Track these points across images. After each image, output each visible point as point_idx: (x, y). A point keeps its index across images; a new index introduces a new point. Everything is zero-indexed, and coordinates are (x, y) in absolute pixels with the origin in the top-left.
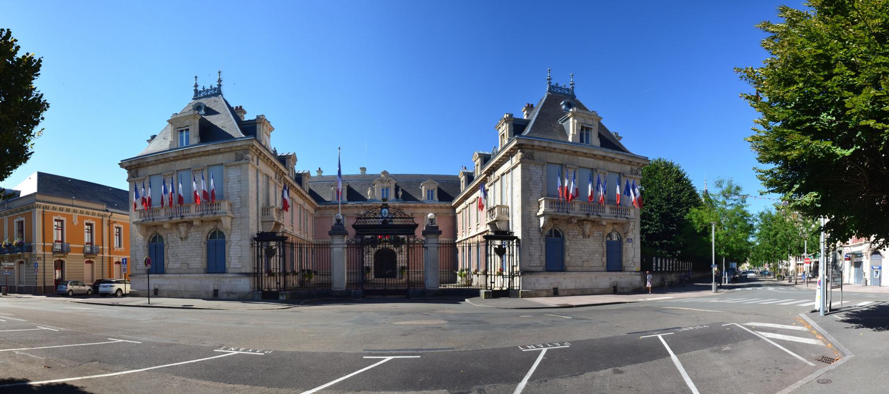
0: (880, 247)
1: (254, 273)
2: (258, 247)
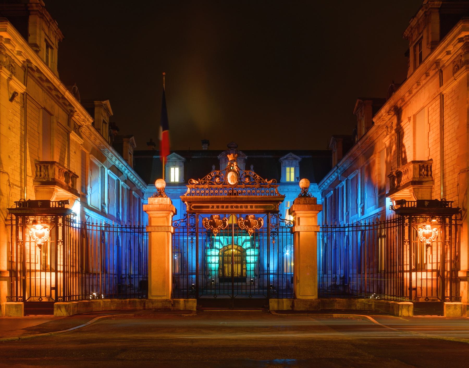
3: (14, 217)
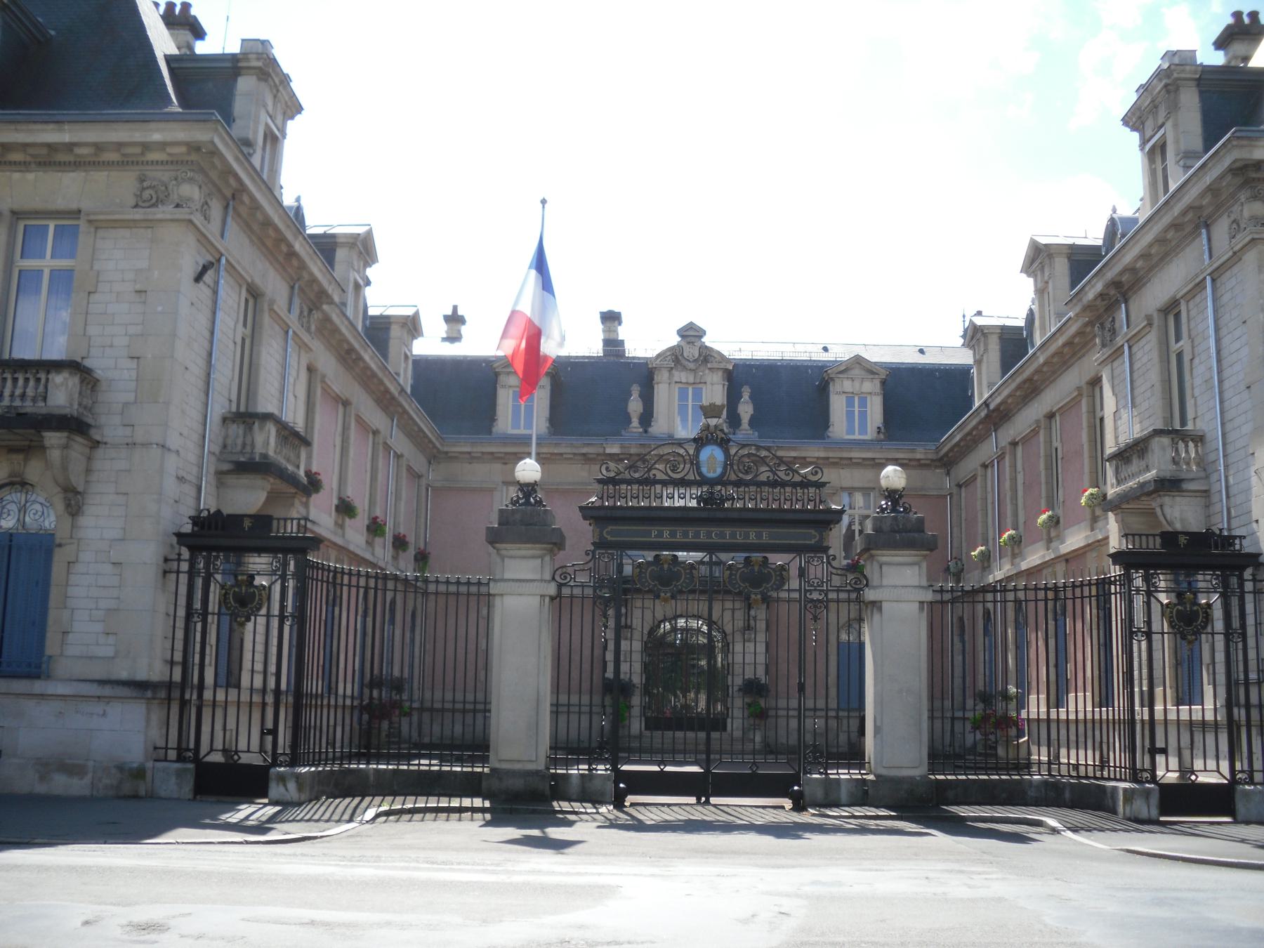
0: (618, 617)
1: (169, 685)
2: (192, 574)
3: (186, 553)
